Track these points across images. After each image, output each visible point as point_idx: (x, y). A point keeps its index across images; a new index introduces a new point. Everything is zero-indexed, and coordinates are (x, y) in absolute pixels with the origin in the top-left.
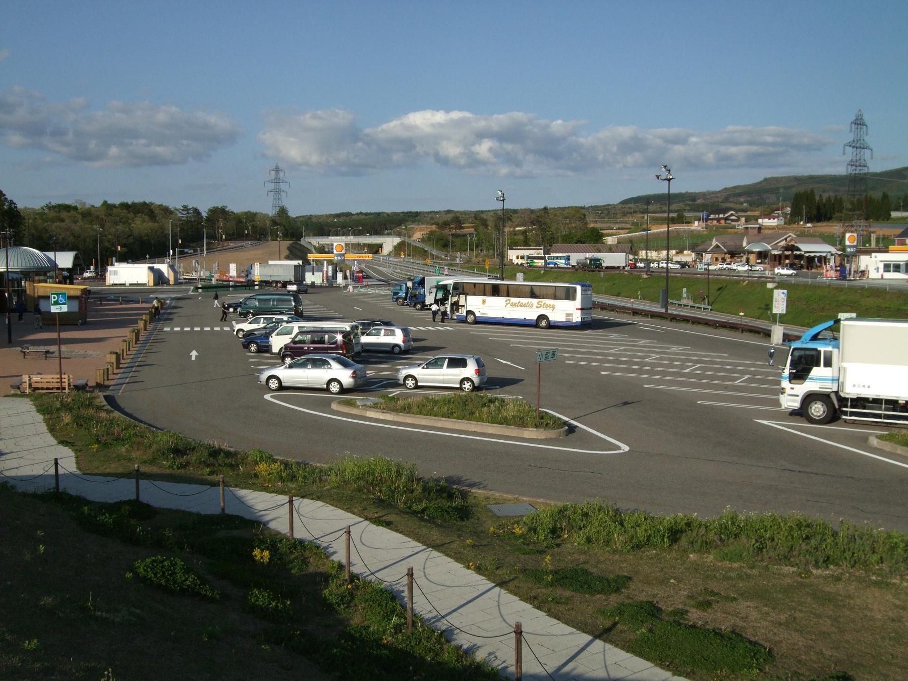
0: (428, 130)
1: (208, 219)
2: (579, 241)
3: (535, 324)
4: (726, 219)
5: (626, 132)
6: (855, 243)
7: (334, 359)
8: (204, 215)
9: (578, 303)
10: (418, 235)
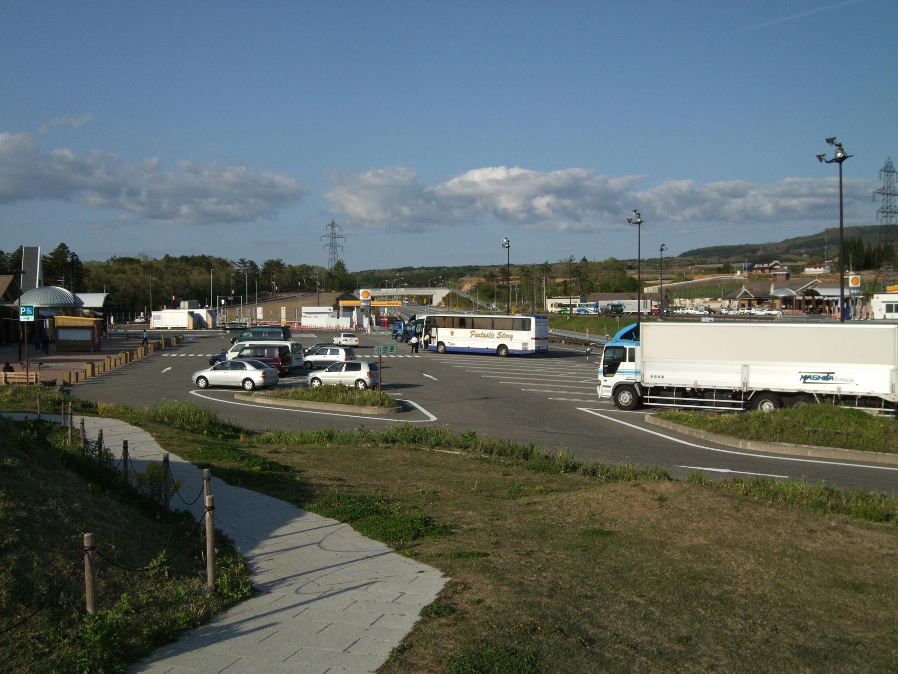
0: (486, 187)
1: (265, 272)
2: (616, 291)
3: (495, 353)
4: (771, 269)
5: (683, 185)
6: (859, 285)
7: (250, 363)
8: (261, 267)
9: (532, 333)
10: (467, 287)
